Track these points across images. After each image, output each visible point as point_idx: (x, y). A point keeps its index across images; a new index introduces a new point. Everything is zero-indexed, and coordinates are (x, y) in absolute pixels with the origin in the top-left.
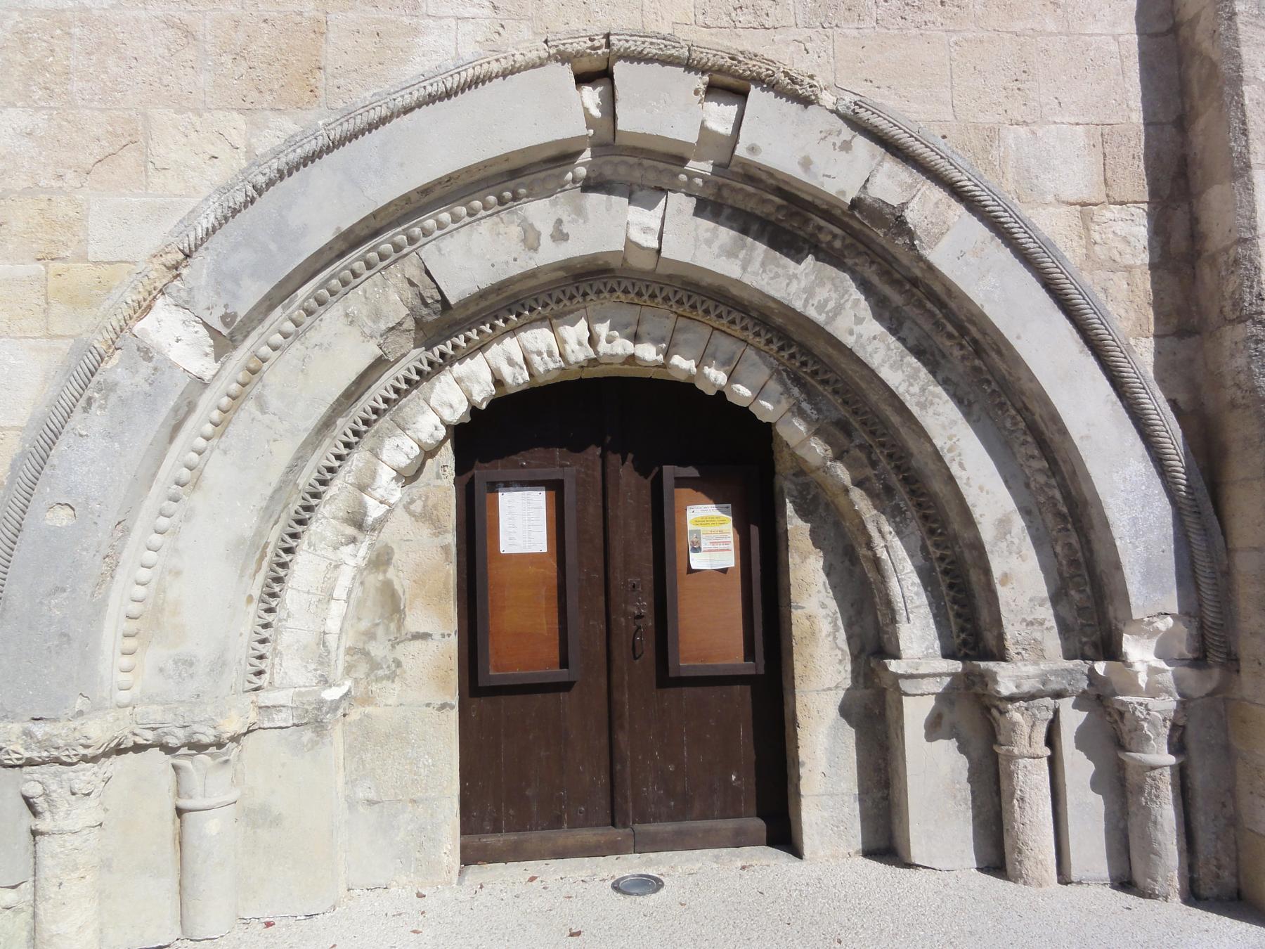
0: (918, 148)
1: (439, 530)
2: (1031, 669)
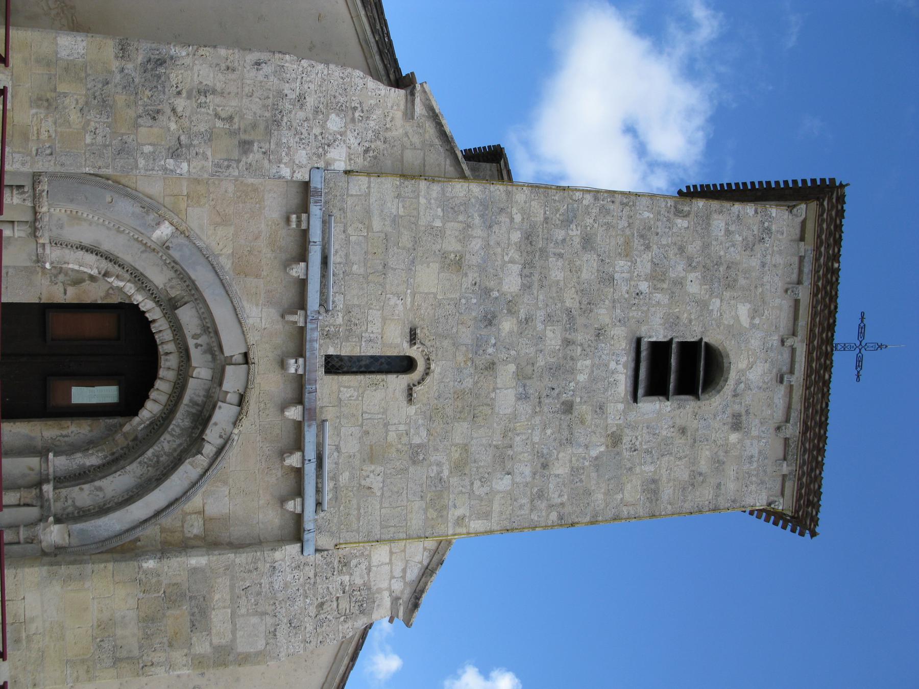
0: (219, 459)
2: (51, 496)
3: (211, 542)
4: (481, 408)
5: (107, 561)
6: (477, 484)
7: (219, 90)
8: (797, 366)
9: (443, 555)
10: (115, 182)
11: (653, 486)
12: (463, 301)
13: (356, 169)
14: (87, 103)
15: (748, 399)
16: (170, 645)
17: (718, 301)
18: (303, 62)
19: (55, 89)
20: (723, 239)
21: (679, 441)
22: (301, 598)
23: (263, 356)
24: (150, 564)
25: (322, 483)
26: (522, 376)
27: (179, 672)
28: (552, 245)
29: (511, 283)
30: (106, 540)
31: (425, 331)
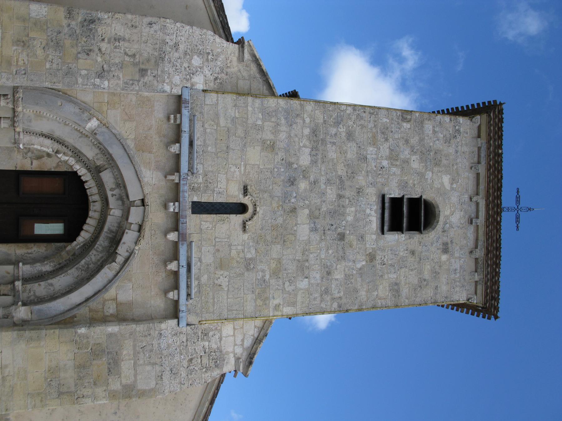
0: (127, 265)
1: (54, 168)
3: (121, 317)
4: (288, 236)
5: (55, 328)
6: (287, 284)
7: (127, 39)
8: (480, 214)
9: (267, 330)
10: (63, 93)
11: (396, 287)
12: (276, 170)
13: (209, 89)
14: (47, 44)
15: (452, 233)
16: (95, 384)
17: (431, 173)
19: (28, 35)
20: (431, 135)
21: (411, 259)
22: (178, 355)
23: (154, 202)
24: (82, 330)
25: (191, 281)
26: (313, 217)
27: (100, 402)
28: (329, 137)
29: (305, 160)
30: (55, 316)
31: (253, 187)
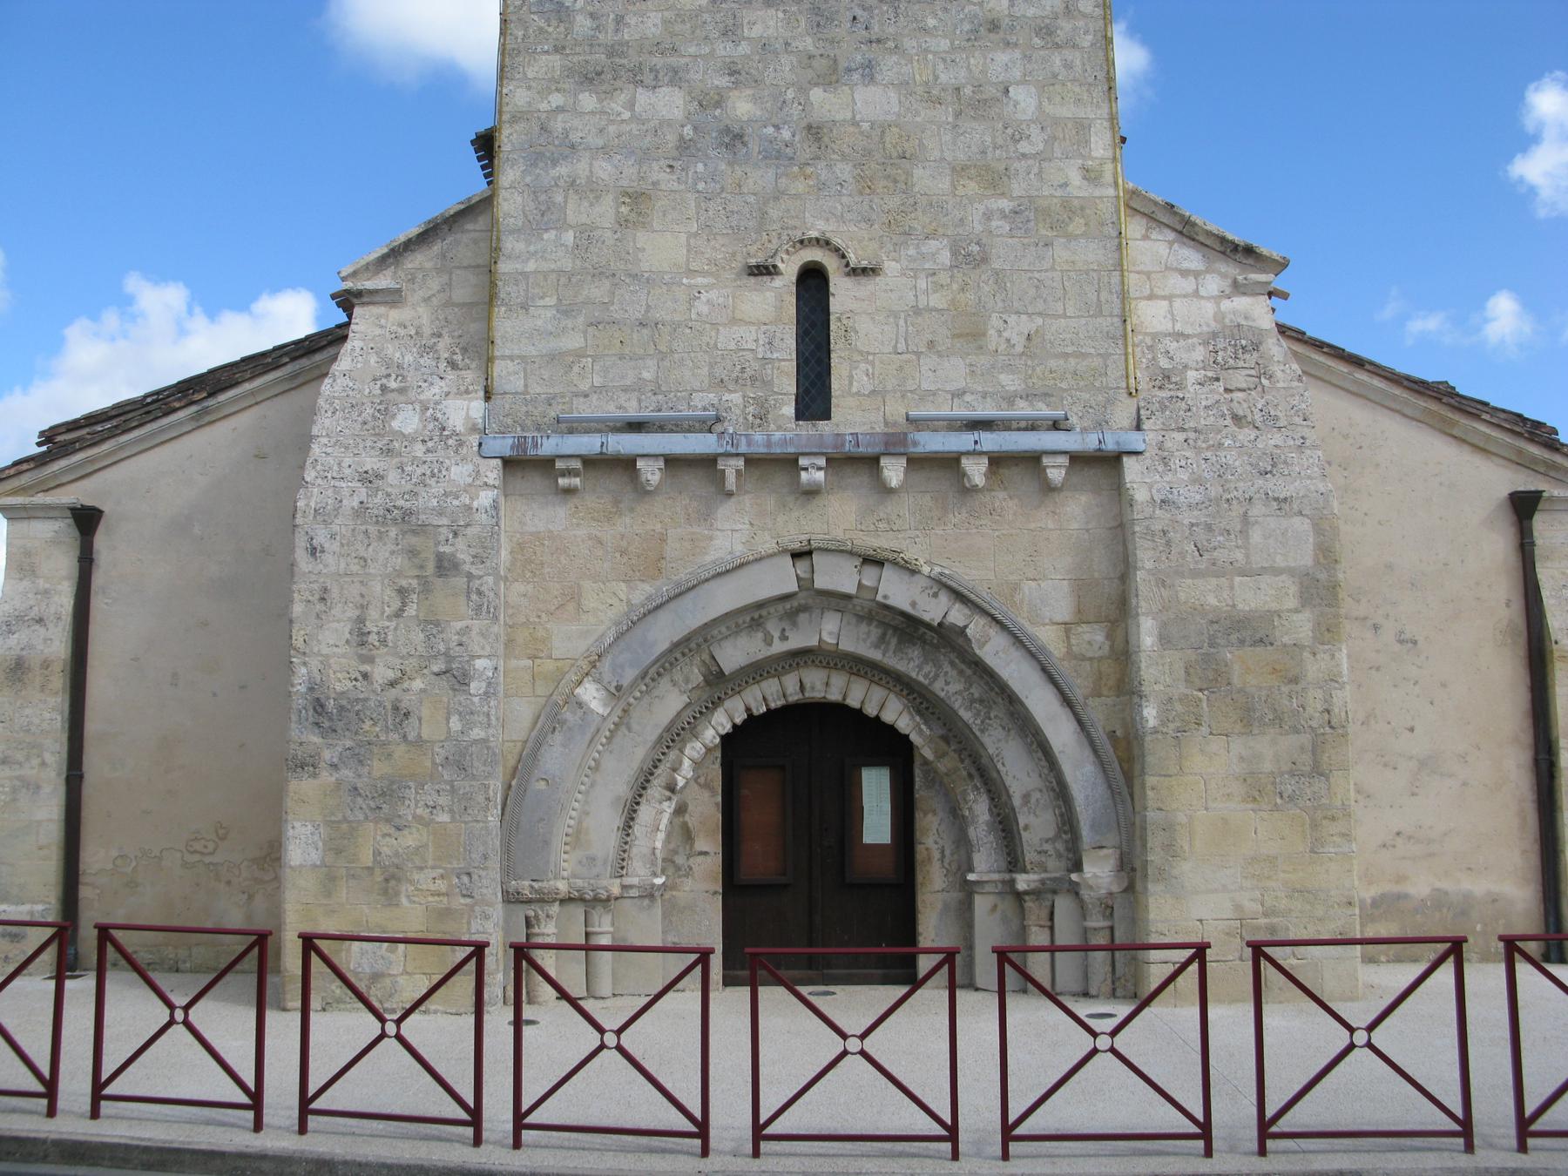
0: (972, 596)
1: (714, 794)
3: (1115, 610)
6: (1024, 147)
7: (357, 613)
9: (1156, 203)
12: (701, 186)
14: (388, 821)
16: (1295, 680)
18: (308, 479)
23: (799, 526)
24: (1150, 714)
25: (1019, 420)
26: (832, 77)
29: (669, 104)
30: (1110, 787)
